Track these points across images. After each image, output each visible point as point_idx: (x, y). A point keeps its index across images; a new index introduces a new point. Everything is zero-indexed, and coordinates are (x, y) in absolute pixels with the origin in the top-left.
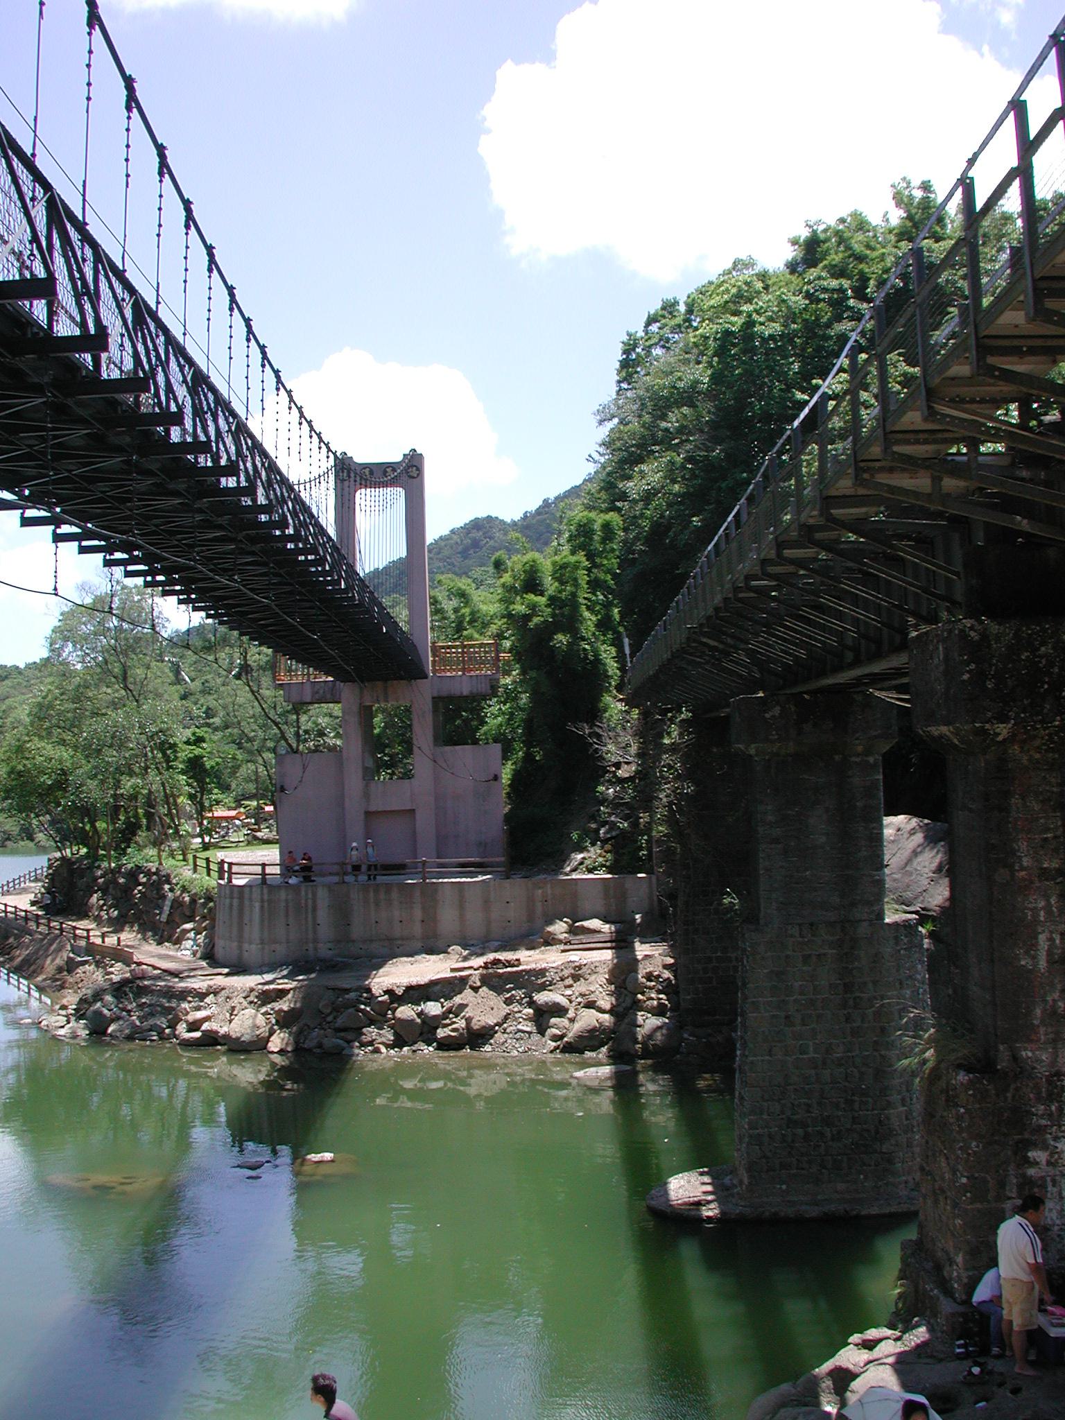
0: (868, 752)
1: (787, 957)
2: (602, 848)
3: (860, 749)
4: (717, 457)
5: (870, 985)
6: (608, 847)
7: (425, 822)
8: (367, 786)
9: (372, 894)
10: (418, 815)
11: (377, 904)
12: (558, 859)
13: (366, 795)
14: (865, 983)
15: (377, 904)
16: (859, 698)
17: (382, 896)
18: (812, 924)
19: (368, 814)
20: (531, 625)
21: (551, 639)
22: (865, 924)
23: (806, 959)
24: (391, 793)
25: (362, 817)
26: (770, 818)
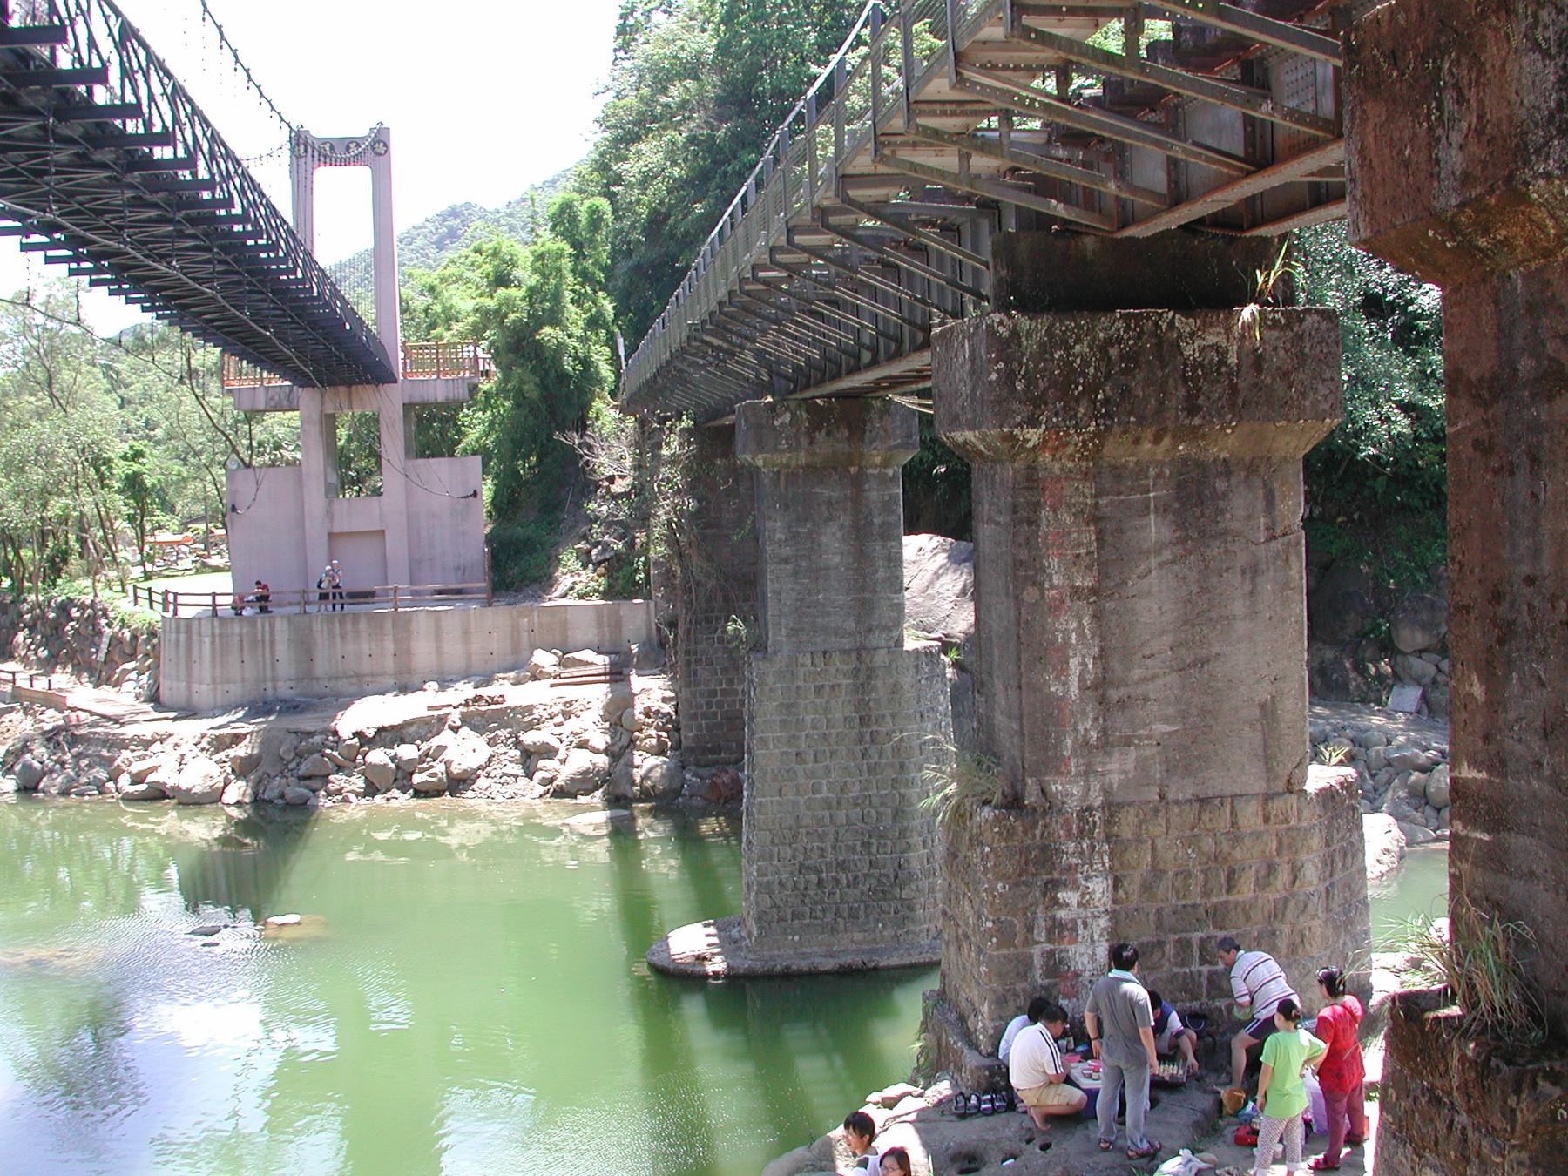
0: (886, 463)
1: (798, 688)
3: (878, 460)
5: (888, 719)
6: (601, 570)
7: (396, 545)
8: (330, 504)
11: (343, 637)
13: (330, 514)
15: (343, 637)
16: (877, 404)
17: (349, 627)
18: (825, 653)
19: (331, 535)
23: (819, 690)
25: (325, 538)
26: (779, 536)
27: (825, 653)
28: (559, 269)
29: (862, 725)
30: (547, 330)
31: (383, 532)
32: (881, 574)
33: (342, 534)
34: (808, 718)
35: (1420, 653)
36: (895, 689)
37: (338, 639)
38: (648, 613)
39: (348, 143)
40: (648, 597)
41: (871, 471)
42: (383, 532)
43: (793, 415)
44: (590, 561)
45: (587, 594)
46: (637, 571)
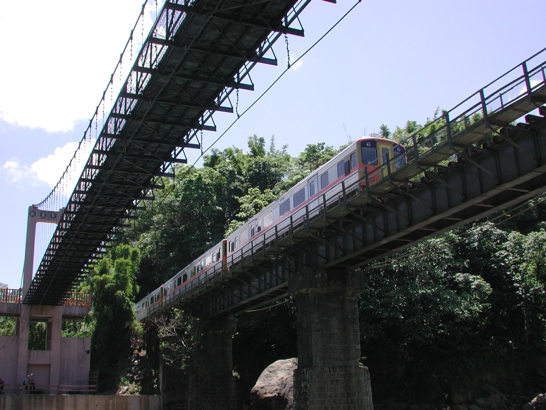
0: (352, 295)
1: (325, 381)
2: (136, 384)
3: (350, 294)
4: (182, 231)
5: (357, 394)
6: (139, 383)
7: (55, 370)
8: (29, 352)
9: (33, 399)
10: (52, 367)
11: (35, 404)
12: (117, 389)
13: (29, 356)
14: (355, 393)
15: (35, 404)
16: (350, 272)
17: (38, 401)
18: (333, 367)
19: (29, 365)
20: (106, 286)
21: (116, 293)
22: (354, 367)
23: (332, 382)
24: (40, 357)
25: (26, 366)
26: (316, 321)
27: (333, 367)
28: (125, 270)
29: (348, 396)
30: (120, 292)
31: (49, 365)
32: (352, 337)
33: (34, 365)
34: (329, 393)
35: (461, 403)
36: (359, 382)
37: (33, 406)
38: (160, 400)
39: (51, 213)
40: (159, 394)
41: (347, 298)
42: (49, 365)
43: (322, 274)
44: (134, 380)
45: (134, 392)
46: (154, 384)
